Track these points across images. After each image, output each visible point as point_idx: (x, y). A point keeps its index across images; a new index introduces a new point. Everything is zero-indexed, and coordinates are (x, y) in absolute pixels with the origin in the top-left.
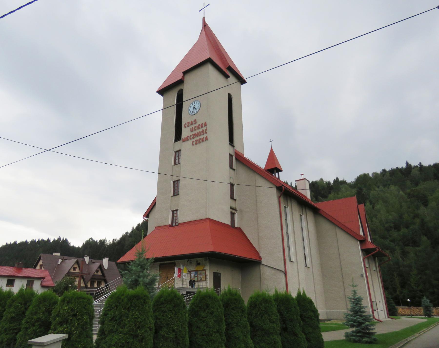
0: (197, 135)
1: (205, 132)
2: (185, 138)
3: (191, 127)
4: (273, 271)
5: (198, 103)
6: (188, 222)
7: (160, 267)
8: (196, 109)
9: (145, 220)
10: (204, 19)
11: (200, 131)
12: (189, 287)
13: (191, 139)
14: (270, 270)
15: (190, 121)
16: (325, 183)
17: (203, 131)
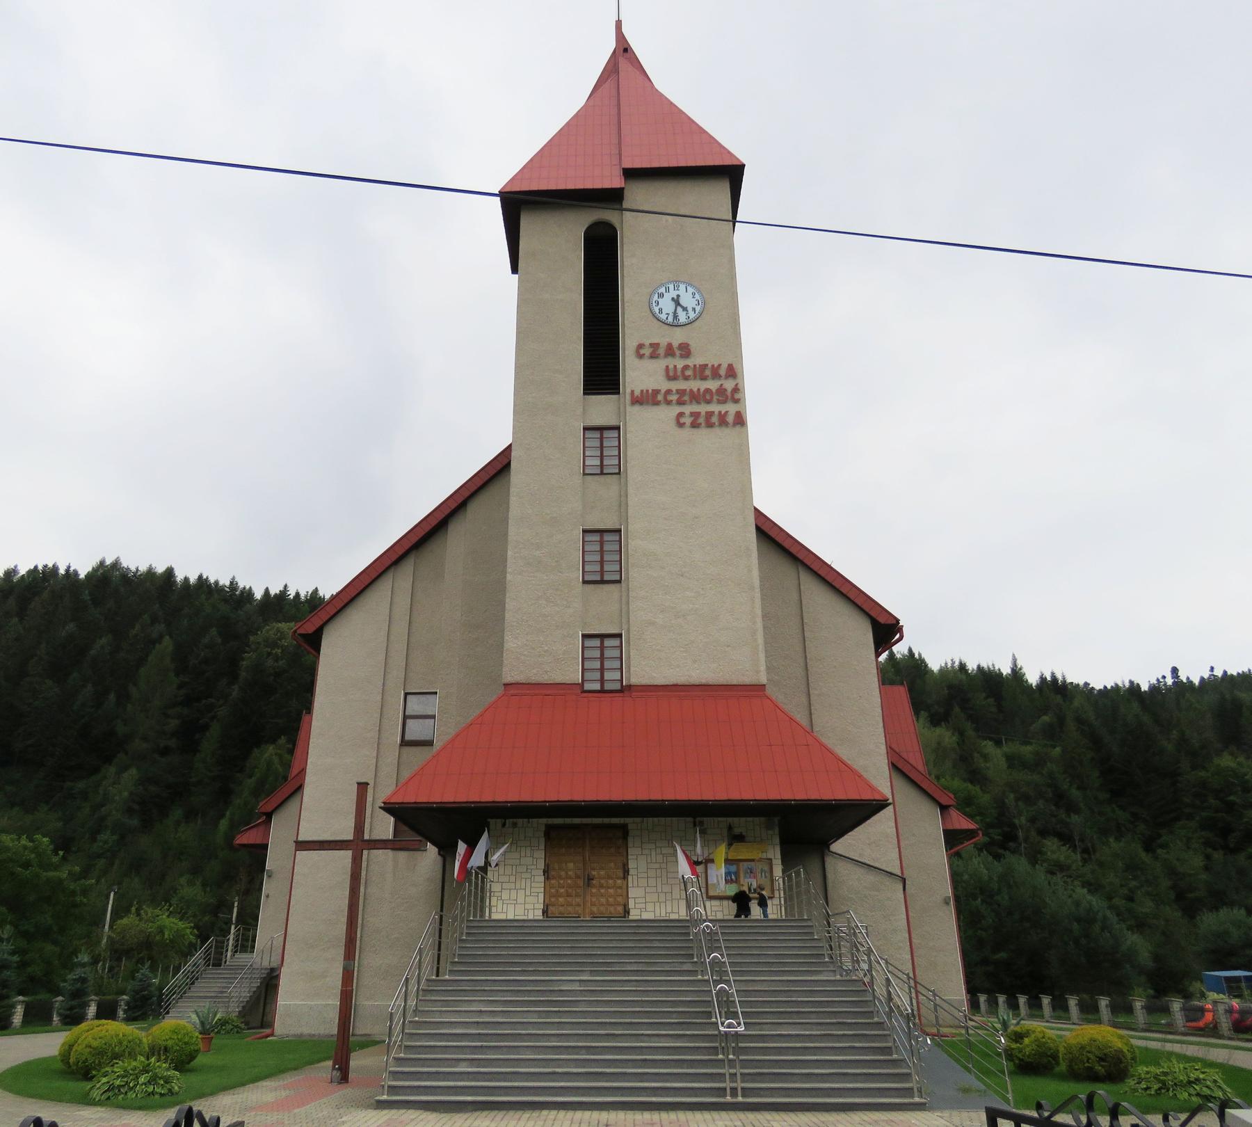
0: (696, 397)
1: (733, 395)
2: (642, 391)
3: (671, 362)
4: (871, 878)
5: (694, 294)
6: (676, 685)
7: (547, 835)
8: (685, 309)
9: (1170, 681)
10: (619, 24)
11: (711, 388)
12: (541, 918)
13: (669, 403)
14: (859, 872)
15: (663, 342)
16: (318, 597)
17: (721, 391)
